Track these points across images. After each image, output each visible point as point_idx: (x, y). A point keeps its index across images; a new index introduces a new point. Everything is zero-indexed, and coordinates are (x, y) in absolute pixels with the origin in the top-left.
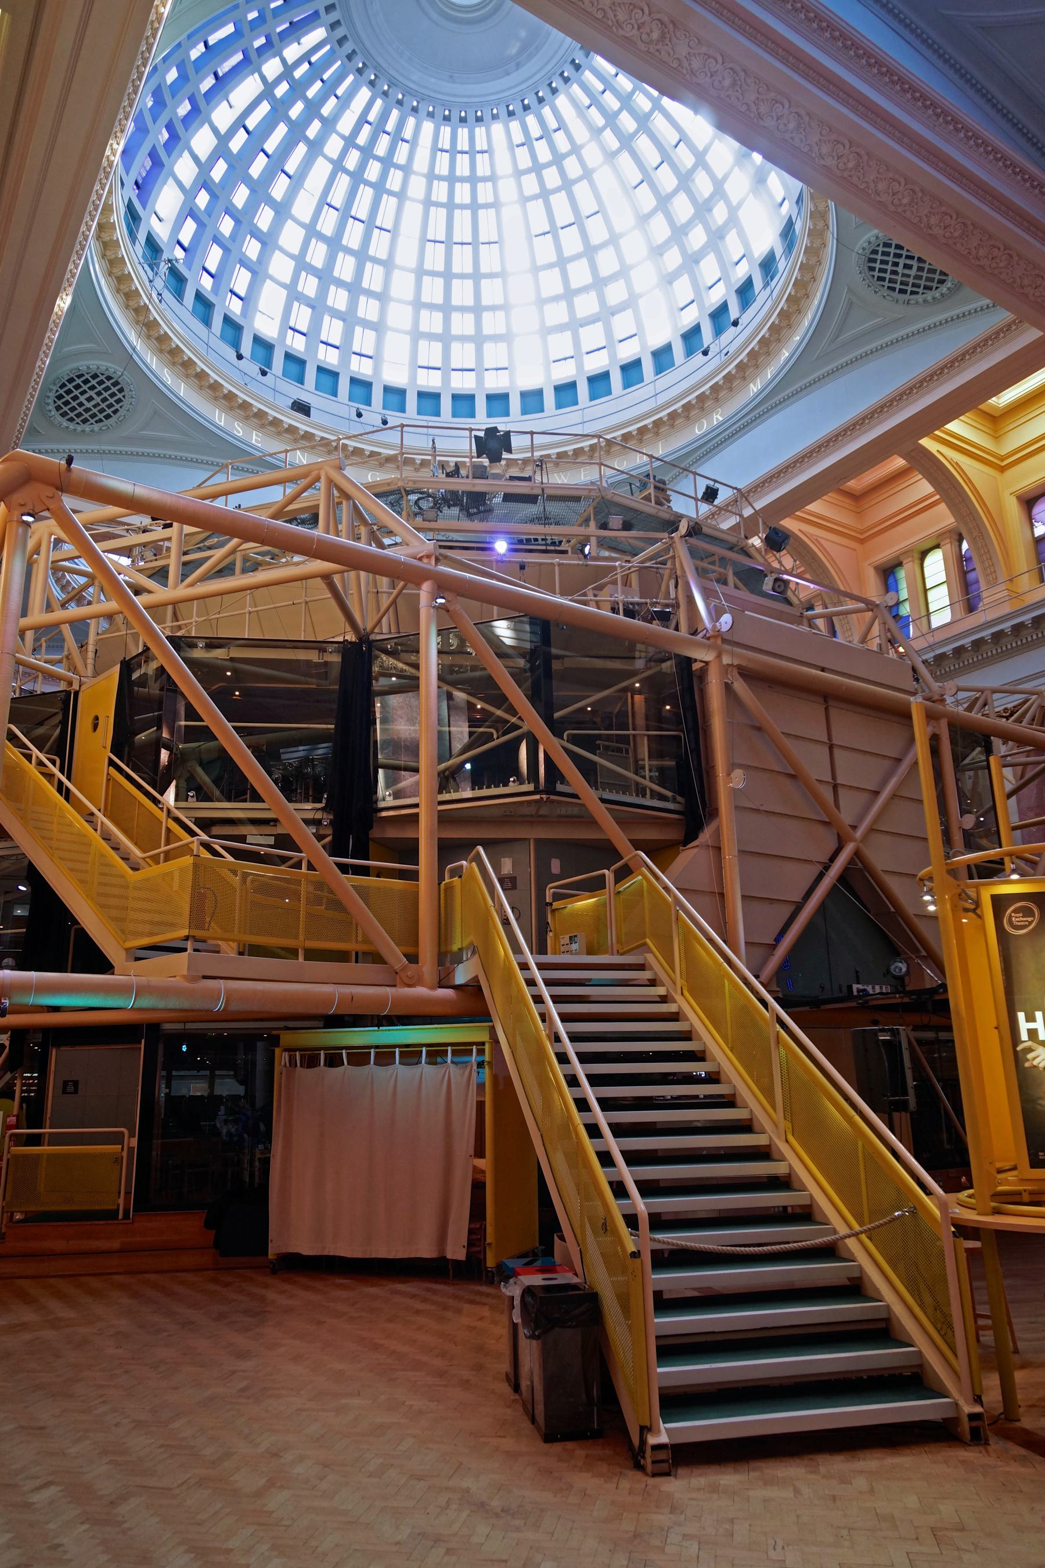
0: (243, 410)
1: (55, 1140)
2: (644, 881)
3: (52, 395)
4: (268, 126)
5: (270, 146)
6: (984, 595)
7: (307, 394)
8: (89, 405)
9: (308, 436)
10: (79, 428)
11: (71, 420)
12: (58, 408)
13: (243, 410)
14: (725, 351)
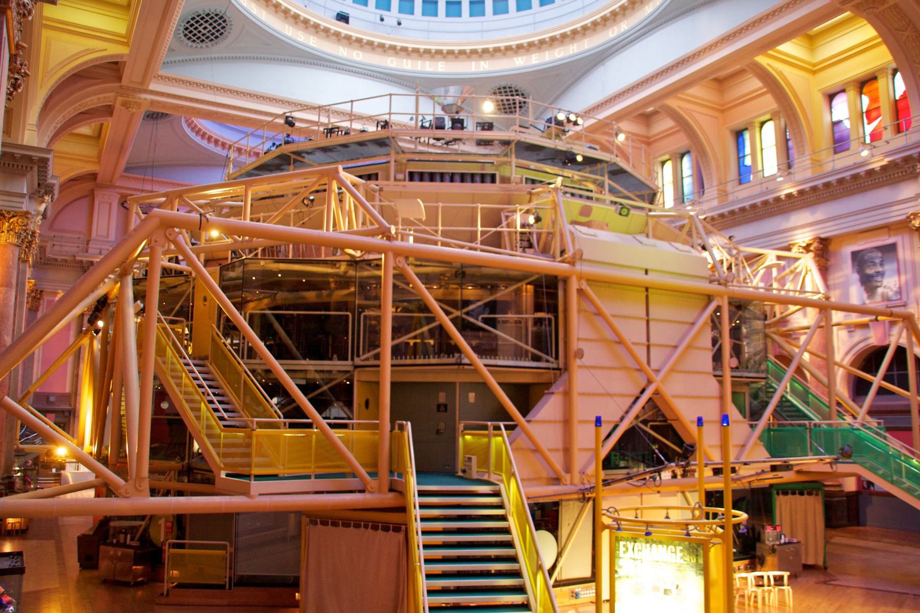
2: (4, 349)
3: (182, 29)
6: (796, 161)
8: (205, 32)
9: (348, 38)
10: (199, 46)
11: (194, 41)
12: (186, 35)
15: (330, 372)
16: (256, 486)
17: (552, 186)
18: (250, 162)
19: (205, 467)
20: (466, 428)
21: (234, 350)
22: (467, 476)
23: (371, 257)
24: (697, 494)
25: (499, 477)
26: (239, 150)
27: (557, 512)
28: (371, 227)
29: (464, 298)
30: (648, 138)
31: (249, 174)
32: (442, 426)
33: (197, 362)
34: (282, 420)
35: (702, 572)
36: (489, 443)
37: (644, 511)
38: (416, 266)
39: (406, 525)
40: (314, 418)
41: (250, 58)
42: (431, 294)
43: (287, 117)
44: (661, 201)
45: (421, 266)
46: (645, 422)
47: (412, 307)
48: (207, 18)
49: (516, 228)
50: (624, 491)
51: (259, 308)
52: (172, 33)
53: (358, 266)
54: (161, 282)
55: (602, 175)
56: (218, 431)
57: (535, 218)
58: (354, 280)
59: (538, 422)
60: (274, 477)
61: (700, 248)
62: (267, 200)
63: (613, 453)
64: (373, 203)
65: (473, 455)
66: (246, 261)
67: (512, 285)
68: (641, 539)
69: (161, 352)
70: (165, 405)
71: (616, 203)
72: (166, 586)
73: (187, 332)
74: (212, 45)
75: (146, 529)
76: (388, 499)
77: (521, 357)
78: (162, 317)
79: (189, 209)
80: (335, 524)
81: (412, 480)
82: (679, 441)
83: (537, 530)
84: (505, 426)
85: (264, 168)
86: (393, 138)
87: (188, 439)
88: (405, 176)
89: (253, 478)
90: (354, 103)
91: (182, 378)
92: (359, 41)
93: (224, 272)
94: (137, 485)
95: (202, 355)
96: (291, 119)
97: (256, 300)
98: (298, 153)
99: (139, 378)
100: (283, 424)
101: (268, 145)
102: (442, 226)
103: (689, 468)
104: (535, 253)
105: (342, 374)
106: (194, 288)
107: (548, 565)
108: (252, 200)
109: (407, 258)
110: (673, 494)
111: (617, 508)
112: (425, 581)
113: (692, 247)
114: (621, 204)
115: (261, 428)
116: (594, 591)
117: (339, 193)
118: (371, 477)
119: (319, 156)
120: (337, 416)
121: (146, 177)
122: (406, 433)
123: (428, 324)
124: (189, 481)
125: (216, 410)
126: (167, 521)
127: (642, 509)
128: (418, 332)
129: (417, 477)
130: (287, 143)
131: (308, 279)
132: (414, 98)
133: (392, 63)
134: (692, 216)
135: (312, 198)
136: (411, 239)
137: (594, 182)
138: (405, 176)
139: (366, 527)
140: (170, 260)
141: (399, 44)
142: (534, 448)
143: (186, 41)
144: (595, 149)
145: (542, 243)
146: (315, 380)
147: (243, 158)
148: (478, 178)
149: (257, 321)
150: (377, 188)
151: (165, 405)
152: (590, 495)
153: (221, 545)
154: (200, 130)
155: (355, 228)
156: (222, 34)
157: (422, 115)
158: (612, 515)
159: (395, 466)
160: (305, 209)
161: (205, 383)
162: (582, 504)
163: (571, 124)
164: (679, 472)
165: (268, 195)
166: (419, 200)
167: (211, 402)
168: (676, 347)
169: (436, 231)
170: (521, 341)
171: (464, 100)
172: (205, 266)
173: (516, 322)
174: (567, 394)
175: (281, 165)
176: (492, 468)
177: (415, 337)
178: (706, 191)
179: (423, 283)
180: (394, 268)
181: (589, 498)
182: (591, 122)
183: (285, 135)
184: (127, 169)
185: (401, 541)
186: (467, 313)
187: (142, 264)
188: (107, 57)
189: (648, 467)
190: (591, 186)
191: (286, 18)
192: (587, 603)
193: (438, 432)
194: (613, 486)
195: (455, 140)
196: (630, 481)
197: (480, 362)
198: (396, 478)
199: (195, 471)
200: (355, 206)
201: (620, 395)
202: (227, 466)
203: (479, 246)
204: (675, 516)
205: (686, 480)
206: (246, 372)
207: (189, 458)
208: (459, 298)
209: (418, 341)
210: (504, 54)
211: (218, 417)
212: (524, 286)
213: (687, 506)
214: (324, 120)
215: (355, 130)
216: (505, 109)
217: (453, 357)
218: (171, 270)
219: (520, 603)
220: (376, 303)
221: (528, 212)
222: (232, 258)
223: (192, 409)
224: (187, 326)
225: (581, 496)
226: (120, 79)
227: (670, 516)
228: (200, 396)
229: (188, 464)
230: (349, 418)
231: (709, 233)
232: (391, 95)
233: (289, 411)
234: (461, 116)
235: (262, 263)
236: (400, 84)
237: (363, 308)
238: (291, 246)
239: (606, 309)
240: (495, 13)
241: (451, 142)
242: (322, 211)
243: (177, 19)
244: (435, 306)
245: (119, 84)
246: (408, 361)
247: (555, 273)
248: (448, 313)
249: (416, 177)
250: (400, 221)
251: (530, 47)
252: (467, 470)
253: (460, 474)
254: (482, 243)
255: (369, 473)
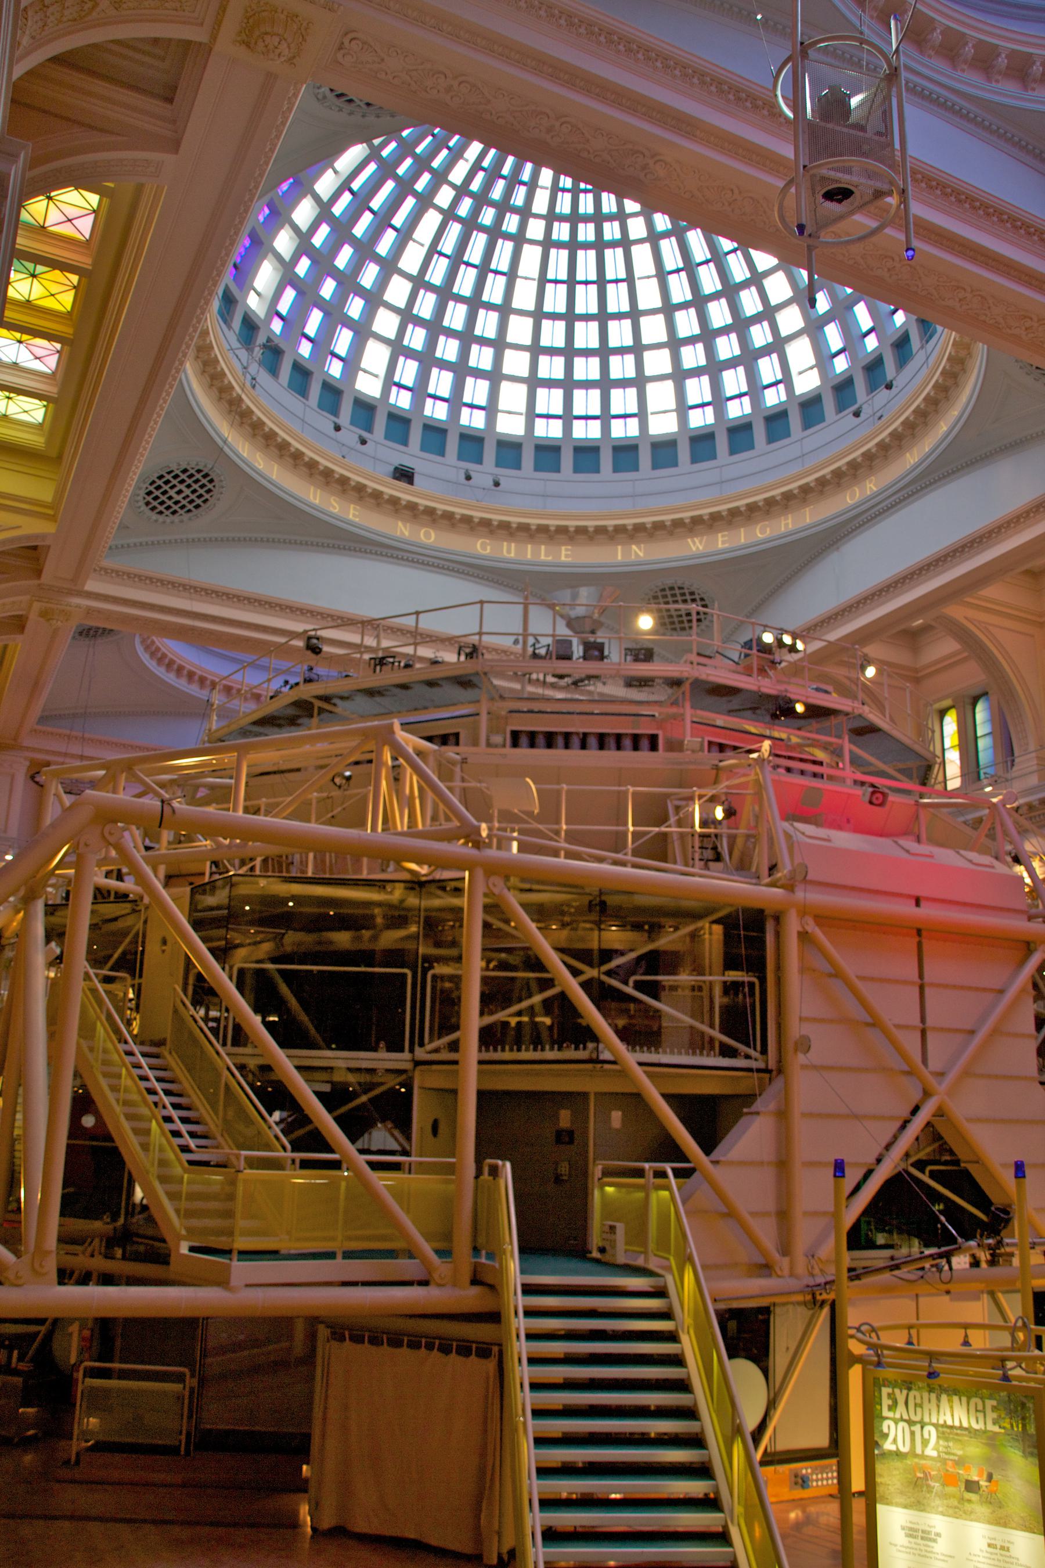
0: (343, 486)
1: (123, 1375)
3: (142, 493)
4: (374, 186)
5: (376, 203)
7: (412, 456)
9: (412, 507)
10: (168, 520)
11: (161, 513)
12: (147, 504)
13: (343, 486)
14: (878, 414)
15: (371, 1071)
16: (240, 1270)
17: (755, 755)
18: (248, 710)
19: (150, 1232)
20: (607, 1173)
21: (211, 1029)
22: (606, 1258)
23: (447, 875)
24: (1018, 1297)
25: (664, 1262)
26: (228, 690)
27: (767, 1323)
28: (447, 825)
29: (605, 946)
30: (916, 671)
31: (244, 733)
32: (564, 1169)
33: (147, 1049)
34: (290, 1154)
35: (1035, 1451)
36: (647, 1198)
37: (922, 1331)
38: (522, 890)
39: (500, 1345)
40: (343, 1153)
41: (250, 540)
42: (546, 937)
43: (309, 638)
44: (940, 778)
45: (530, 890)
46: (920, 1165)
47: (513, 959)
48: (183, 476)
49: (693, 826)
50: (887, 1290)
51: (254, 958)
52: (126, 500)
53: (424, 890)
54: (93, 912)
55: (839, 737)
56: (178, 1170)
57: (724, 811)
58: (416, 913)
59: (731, 1163)
60: (273, 1254)
61: (1009, 859)
62: (272, 776)
63: (863, 1219)
64: (450, 784)
65: (618, 1221)
66: (234, 879)
67: (686, 924)
68: (920, 1384)
69: (87, 1030)
70: (88, 1121)
71: (863, 784)
72: (76, 1445)
73: (131, 995)
74: (190, 519)
75: (49, 1336)
76: (470, 1298)
77: (702, 1049)
78: (91, 971)
79: (140, 789)
80: (375, 1341)
81: (513, 1265)
82: (982, 1200)
83: (731, 1356)
84: (674, 1170)
85: (269, 721)
86: (485, 674)
87: (125, 1181)
88: (505, 740)
89: (235, 1255)
90: (421, 616)
91: (119, 1076)
92: (430, 512)
93: (198, 897)
94: (37, 1266)
95: (157, 1037)
96: (315, 641)
97: (249, 944)
98: (326, 699)
99: (49, 1074)
100: (290, 1162)
101: (276, 684)
102: (566, 824)
103: (1002, 1250)
104: (726, 870)
105: (393, 1076)
106: (145, 922)
107: (751, 1423)
108: (248, 775)
109: (507, 878)
110: (976, 1297)
111: (876, 1324)
112: (533, 1451)
113: (997, 858)
114: (873, 786)
115: (251, 1167)
116: (835, 1474)
117: (394, 767)
118: (440, 1257)
119: (362, 703)
120: (382, 1147)
121: (74, 733)
122: (502, 1182)
123: (542, 990)
124: (124, 1258)
125: (176, 1134)
126: (81, 1328)
127: (918, 1327)
128: (525, 1004)
129: (520, 1259)
130: (308, 681)
131: (338, 911)
132: (521, 607)
133: (482, 547)
134: (994, 804)
135: (348, 774)
136: (515, 845)
137: (825, 747)
138: (505, 740)
139: (430, 1347)
140: (108, 874)
141: (496, 518)
142: (724, 1209)
143: (149, 513)
144: (826, 692)
145: (736, 853)
146: (346, 1085)
147: (235, 704)
148: (627, 742)
149: (249, 980)
150: (458, 757)
151: (88, 1121)
152: (824, 1296)
153: (172, 1373)
154: (164, 656)
155: (420, 826)
156: (206, 501)
157: (535, 636)
158: (867, 1339)
159: (481, 1240)
160: (336, 793)
161: (158, 1087)
162: (811, 1312)
163: (785, 651)
164: (983, 1256)
165: (275, 769)
166: (528, 780)
167: (168, 1119)
168: (972, 1032)
169: (557, 833)
170: (702, 1022)
171: (603, 611)
172: (166, 885)
173: (693, 989)
174: (783, 1115)
175: (299, 717)
176: (652, 1245)
177: (519, 1014)
178: (1017, 760)
179: (533, 920)
180: (486, 895)
181: (823, 1302)
182: (817, 645)
183: (305, 667)
184: (43, 719)
185: (491, 1374)
186: (609, 973)
187: (61, 880)
188: (19, 538)
189: (927, 1245)
190: (820, 755)
191: (311, 475)
192: (822, 1497)
193: (558, 1179)
194: (867, 1280)
195: (589, 677)
196: (896, 1272)
197: (630, 1058)
198: (483, 1260)
199: (135, 1239)
200: (421, 789)
201: (875, 1117)
202: (191, 1232)
203: (629, 858)
204: (980, 1341)
205: (996, 1270)
206: (229, 1069)
207: (126, 1214)
208: (595, 946)
209: (525, 1019)
210: (671, 533)
211: (179, 1146)
212: (707, 925)
213: (1001, 1323)
214: (370, 641)
215: (422, 659)
216: (673, 623)
217: (585, 1048)
218: (109, 892)
219: (701, 1496)
220: (453, 952)
221: (713, 800)
222: (211, 874)
223: (136, 1132)
224: (133, 986)
225: (809, 1297)
226: (39, 573)
227: (970, 1341)
228: (150, 1109)
229: (124, 1225)
230: (405, 1153)
231: (1023, 832)
232: (482, 602)
233: (299, 1139)
234: (601, 637)
235: (262, 882)
236: (497, 582)
237: (430, 961)
238: (311, 855)
239: (850, 965)
240: (655, 466)
241: (582, 680)
242: (364, 800)
243: (136, 478)
244: (554, 960)
245: (36, 582)
246: (507, 1055)
247: (757, 905)
248: (575, 972)
249: (524, 740)
250: (496, 814)
251: (714, 522)
252: (608, 1248)
253: (595, 1254)
254: (636, 853)
255: (437, 1252)
